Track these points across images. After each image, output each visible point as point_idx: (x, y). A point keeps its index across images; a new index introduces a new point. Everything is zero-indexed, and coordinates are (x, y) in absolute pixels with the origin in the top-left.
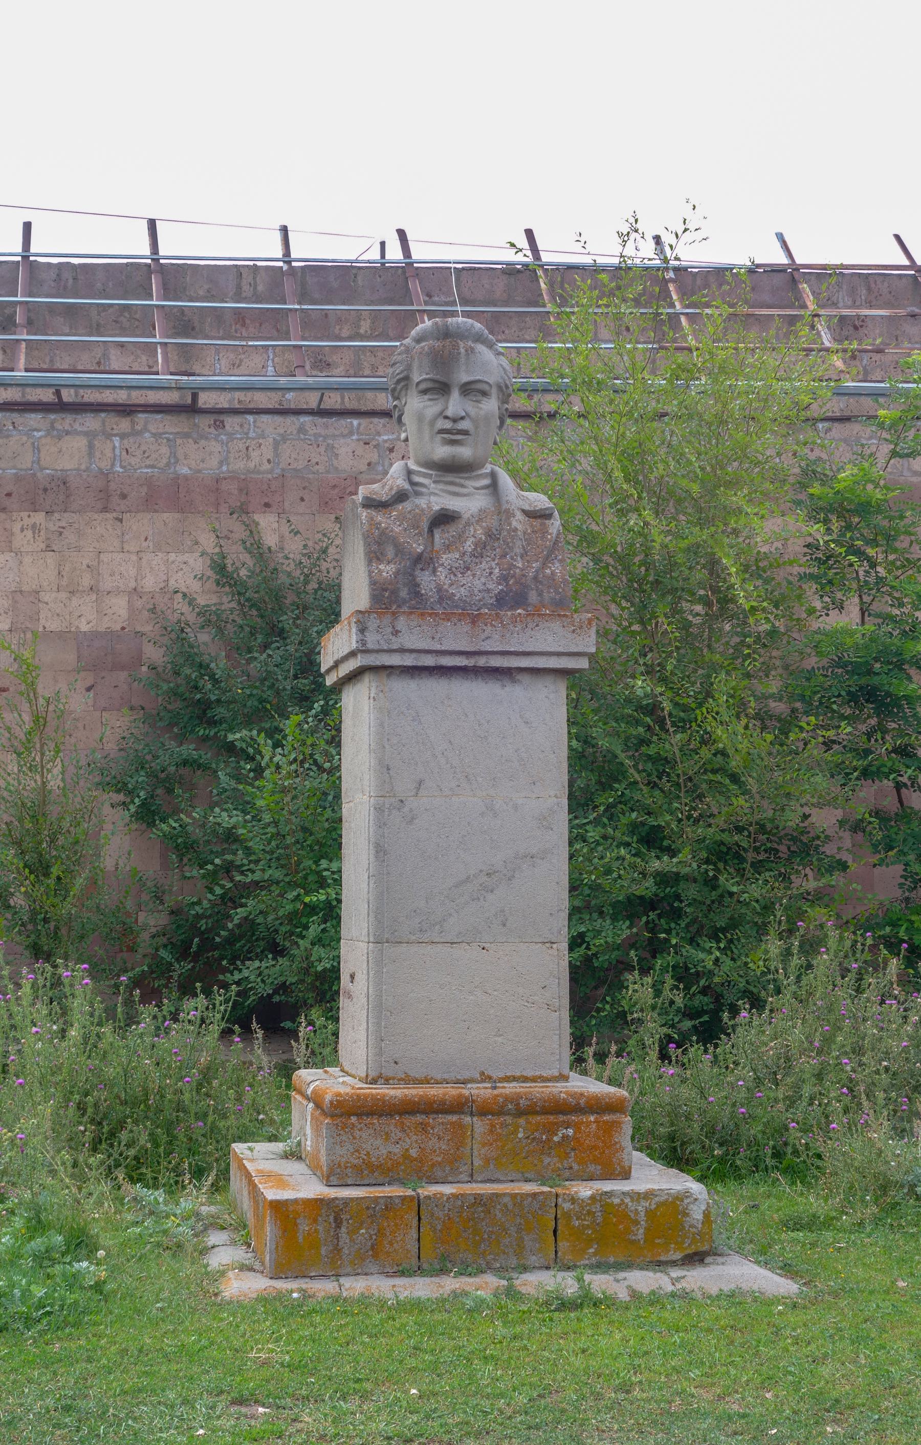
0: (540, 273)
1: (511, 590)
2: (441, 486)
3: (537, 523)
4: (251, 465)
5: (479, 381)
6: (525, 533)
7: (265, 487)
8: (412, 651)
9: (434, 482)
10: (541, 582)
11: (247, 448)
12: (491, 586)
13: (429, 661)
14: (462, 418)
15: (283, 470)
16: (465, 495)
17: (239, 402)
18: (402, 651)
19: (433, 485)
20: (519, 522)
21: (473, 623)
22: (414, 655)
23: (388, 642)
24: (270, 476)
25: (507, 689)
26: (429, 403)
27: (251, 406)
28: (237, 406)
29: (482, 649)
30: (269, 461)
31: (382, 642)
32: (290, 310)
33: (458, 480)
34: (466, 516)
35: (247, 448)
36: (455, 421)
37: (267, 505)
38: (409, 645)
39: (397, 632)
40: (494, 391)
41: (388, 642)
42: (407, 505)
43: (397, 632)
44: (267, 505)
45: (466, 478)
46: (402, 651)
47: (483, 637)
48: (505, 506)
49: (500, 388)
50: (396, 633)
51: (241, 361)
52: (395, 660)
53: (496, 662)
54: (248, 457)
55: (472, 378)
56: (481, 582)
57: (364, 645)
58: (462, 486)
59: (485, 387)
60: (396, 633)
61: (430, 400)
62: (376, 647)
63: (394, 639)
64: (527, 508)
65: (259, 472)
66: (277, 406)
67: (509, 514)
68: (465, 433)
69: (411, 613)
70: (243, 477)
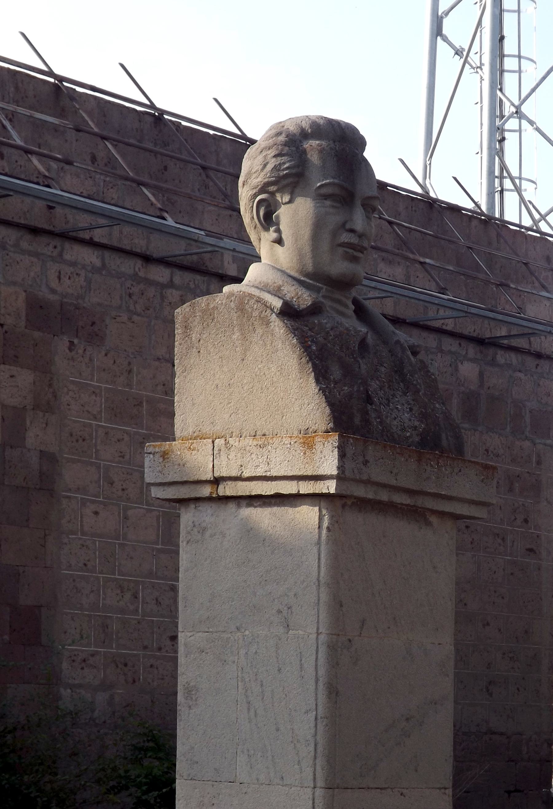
18: (368, 482)
26: (331, 210)
46: (368, 482)
57: (343, 472)
61: (333, 207)
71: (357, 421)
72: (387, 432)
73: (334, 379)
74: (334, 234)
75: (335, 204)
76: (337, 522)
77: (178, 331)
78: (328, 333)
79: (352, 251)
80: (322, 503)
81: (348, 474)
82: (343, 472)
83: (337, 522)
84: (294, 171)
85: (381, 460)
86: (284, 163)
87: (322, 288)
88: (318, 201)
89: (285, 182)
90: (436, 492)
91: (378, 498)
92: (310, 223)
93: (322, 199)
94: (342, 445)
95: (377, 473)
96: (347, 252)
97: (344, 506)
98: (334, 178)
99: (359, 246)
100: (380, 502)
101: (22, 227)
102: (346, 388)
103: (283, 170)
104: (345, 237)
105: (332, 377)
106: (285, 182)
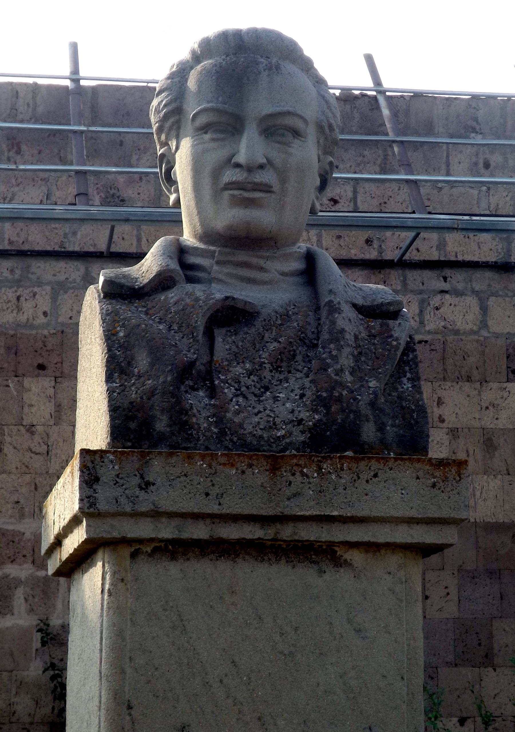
0: (381, 100)
1: (334, 422)
2: (229, 269)
3: (376, 324)
4: (22, 318)
5: (289, 113)
6: (356, 337)
7: (40, 344)
8: (171, 515)
9: (218, 263)
10: (382, 411)
11: (18, 298)
12: (304, 415)
13: (200, 531)
14: (261, 167)
15: (63, 324)
16: (265, 283)
17: (11, 242)
18: (156, 514)
19: (215, 268)
20: (348, 321)
21: (274, 469)
22: (176, 522)
23: (133, 500)
24: (46, 332)
25: (327, 576)
26: (213, 145)
27: (26, 247)
28: (8, 247)
29: (287, 512)
30: (45, 314)
31: (123, 500)
32: (75, 132)
33: (254, 261)
34: (265, 312)
35: (18, 298)
36: (250, 169)
37: (41, 367)
38: (166, 505)
39: (148, 484)
40: (311, 132)
41: (133, 500)
42: (172, 296)
43: (148, 484)
44: (41, 367)
45: (267, 258)
46: (156, 514)
47: (288, 492)
48: (325, 299)
49: (320, 127)
50: (146, 485)
51: (14, 195)
52: (144, 529)
53: (309, 533)
54: (19, 309)
55: (278, 109)
56: (288, 406)
57: (92, 505)
58: (261, 269)
59: (299, 124)
60: (146, 485)
61: (213, 140)
62: (113, 508)
63: (142, 495)
64: (360, 302)
65: (32, 327)
66: (57, 248)
67: (333, 309)
68: (267, 189)
69: (171, 455)
70: (12, 332)
71: (162, 425)
72: (232, 435)
73: (139, 372)
74: (216, 174)
75: (215, 136)
76: (122, 580)
77: (79, 343)
78: (169, 308)
79: (241, 192)
80: (106, 556)
81: (102, 506)
82: (92, 505)
83: (122, 580)
84: (170, 108)
85: (183, 479)
86: (162, 101)
87: (215, 252)
88: (196, 137)
89: (167, 125)
90: (318, 513)
91: (185, 535)
92: (190, 168)
93: (201, 134)
94: (90, 465)
95: (168, 498)
96: (233, 196)
97: (134, 555)
98: (208, 102)
99: (249, 183)
100: (221, 541)
101: (65, 256)
102: (150, 382)
103: (162, 110)
104: (230, 175)
105: (136, 370)
106: (167, 125)
